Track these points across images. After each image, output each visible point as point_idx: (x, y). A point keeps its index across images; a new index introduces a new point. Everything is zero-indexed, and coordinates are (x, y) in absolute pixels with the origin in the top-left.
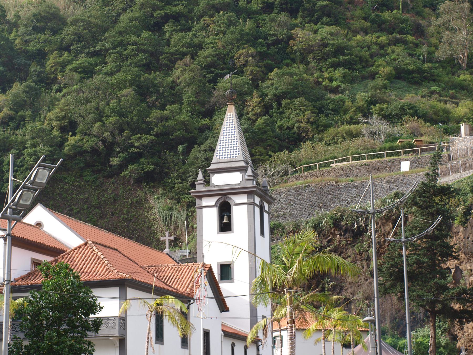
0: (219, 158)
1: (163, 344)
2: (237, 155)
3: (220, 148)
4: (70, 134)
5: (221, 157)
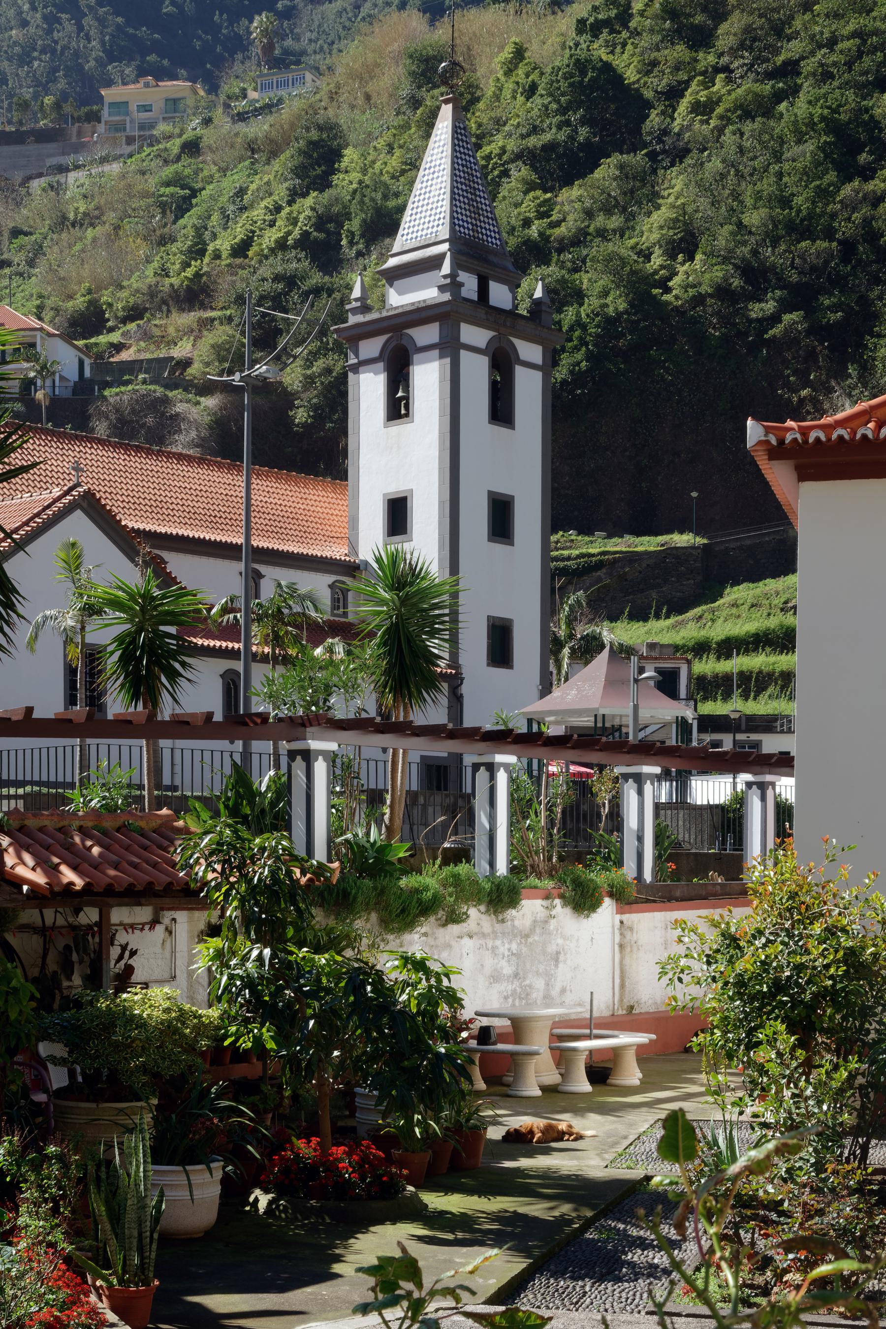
4: (680, 257)
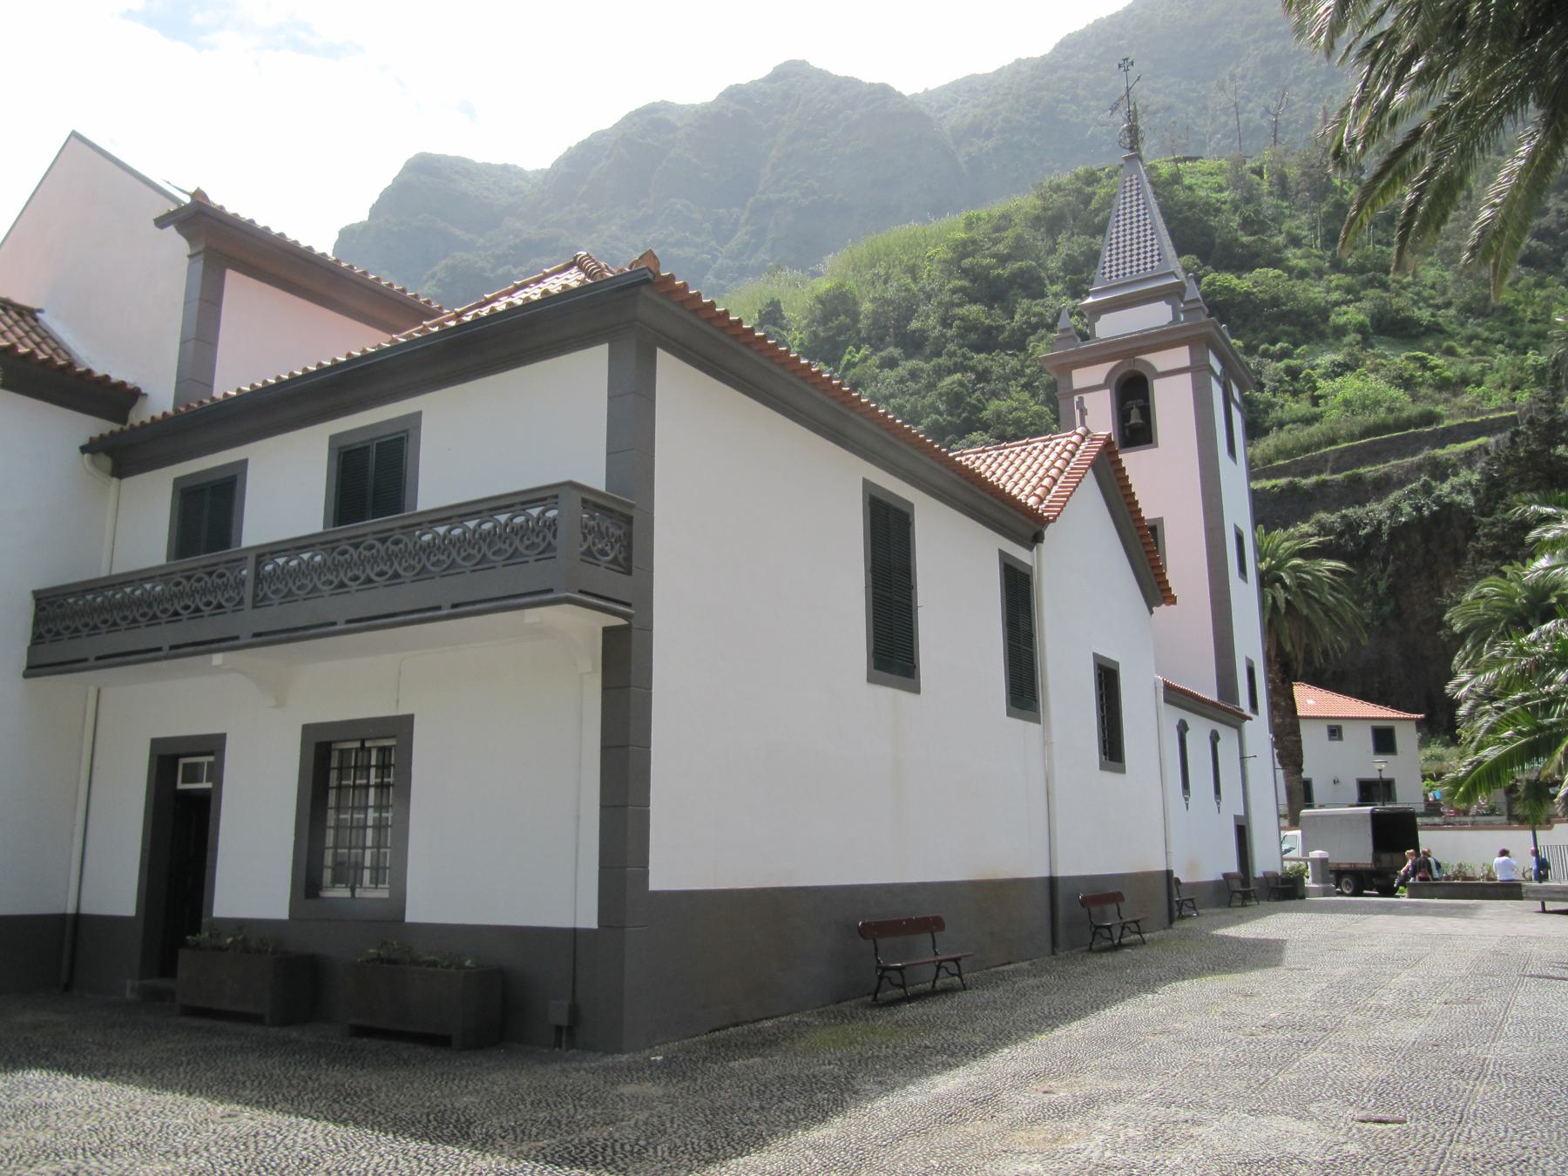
0: (1111, 277)
1: (1122, 771)
2: (1156, 264)
3: (1111, 255)
5: (1114, 274)
